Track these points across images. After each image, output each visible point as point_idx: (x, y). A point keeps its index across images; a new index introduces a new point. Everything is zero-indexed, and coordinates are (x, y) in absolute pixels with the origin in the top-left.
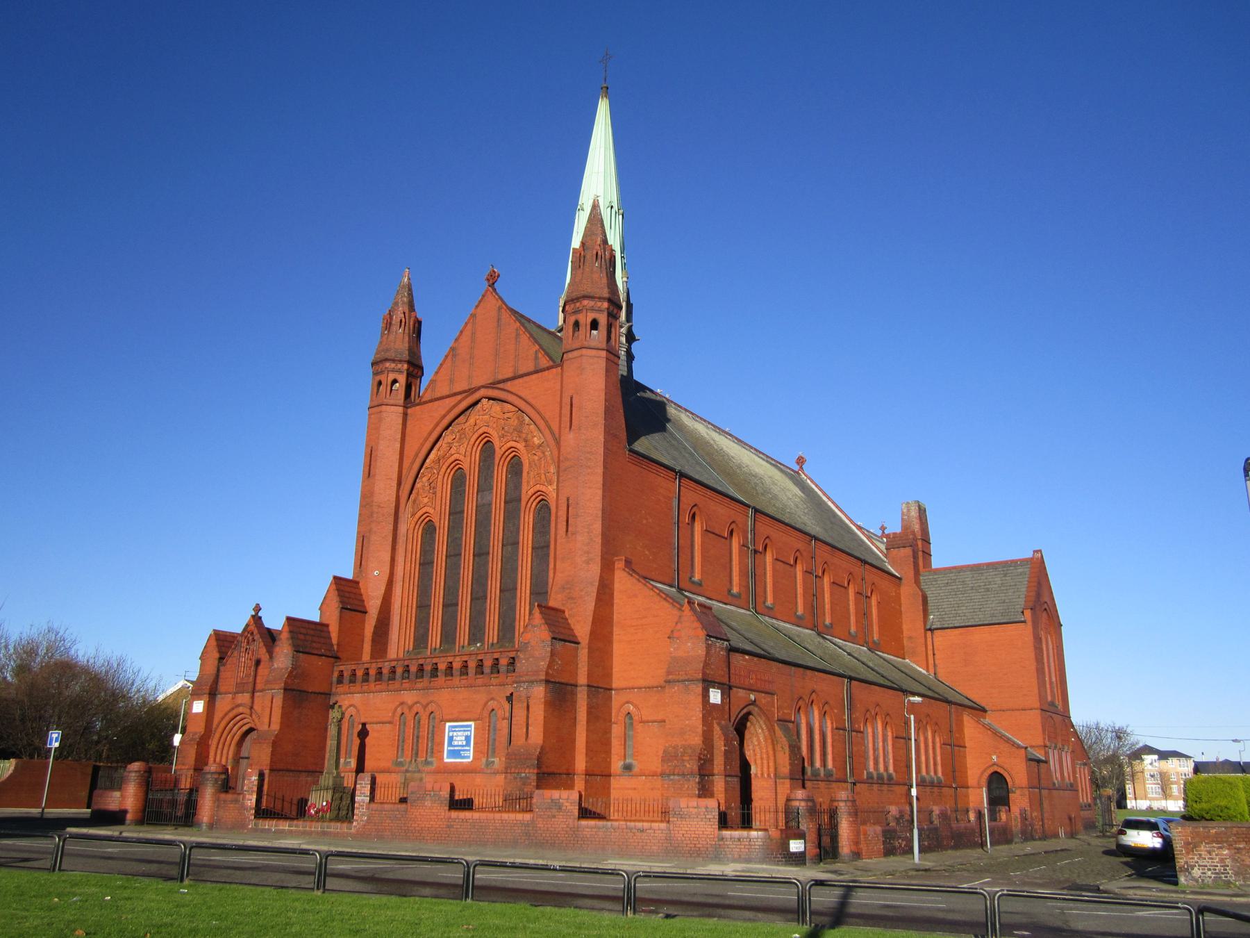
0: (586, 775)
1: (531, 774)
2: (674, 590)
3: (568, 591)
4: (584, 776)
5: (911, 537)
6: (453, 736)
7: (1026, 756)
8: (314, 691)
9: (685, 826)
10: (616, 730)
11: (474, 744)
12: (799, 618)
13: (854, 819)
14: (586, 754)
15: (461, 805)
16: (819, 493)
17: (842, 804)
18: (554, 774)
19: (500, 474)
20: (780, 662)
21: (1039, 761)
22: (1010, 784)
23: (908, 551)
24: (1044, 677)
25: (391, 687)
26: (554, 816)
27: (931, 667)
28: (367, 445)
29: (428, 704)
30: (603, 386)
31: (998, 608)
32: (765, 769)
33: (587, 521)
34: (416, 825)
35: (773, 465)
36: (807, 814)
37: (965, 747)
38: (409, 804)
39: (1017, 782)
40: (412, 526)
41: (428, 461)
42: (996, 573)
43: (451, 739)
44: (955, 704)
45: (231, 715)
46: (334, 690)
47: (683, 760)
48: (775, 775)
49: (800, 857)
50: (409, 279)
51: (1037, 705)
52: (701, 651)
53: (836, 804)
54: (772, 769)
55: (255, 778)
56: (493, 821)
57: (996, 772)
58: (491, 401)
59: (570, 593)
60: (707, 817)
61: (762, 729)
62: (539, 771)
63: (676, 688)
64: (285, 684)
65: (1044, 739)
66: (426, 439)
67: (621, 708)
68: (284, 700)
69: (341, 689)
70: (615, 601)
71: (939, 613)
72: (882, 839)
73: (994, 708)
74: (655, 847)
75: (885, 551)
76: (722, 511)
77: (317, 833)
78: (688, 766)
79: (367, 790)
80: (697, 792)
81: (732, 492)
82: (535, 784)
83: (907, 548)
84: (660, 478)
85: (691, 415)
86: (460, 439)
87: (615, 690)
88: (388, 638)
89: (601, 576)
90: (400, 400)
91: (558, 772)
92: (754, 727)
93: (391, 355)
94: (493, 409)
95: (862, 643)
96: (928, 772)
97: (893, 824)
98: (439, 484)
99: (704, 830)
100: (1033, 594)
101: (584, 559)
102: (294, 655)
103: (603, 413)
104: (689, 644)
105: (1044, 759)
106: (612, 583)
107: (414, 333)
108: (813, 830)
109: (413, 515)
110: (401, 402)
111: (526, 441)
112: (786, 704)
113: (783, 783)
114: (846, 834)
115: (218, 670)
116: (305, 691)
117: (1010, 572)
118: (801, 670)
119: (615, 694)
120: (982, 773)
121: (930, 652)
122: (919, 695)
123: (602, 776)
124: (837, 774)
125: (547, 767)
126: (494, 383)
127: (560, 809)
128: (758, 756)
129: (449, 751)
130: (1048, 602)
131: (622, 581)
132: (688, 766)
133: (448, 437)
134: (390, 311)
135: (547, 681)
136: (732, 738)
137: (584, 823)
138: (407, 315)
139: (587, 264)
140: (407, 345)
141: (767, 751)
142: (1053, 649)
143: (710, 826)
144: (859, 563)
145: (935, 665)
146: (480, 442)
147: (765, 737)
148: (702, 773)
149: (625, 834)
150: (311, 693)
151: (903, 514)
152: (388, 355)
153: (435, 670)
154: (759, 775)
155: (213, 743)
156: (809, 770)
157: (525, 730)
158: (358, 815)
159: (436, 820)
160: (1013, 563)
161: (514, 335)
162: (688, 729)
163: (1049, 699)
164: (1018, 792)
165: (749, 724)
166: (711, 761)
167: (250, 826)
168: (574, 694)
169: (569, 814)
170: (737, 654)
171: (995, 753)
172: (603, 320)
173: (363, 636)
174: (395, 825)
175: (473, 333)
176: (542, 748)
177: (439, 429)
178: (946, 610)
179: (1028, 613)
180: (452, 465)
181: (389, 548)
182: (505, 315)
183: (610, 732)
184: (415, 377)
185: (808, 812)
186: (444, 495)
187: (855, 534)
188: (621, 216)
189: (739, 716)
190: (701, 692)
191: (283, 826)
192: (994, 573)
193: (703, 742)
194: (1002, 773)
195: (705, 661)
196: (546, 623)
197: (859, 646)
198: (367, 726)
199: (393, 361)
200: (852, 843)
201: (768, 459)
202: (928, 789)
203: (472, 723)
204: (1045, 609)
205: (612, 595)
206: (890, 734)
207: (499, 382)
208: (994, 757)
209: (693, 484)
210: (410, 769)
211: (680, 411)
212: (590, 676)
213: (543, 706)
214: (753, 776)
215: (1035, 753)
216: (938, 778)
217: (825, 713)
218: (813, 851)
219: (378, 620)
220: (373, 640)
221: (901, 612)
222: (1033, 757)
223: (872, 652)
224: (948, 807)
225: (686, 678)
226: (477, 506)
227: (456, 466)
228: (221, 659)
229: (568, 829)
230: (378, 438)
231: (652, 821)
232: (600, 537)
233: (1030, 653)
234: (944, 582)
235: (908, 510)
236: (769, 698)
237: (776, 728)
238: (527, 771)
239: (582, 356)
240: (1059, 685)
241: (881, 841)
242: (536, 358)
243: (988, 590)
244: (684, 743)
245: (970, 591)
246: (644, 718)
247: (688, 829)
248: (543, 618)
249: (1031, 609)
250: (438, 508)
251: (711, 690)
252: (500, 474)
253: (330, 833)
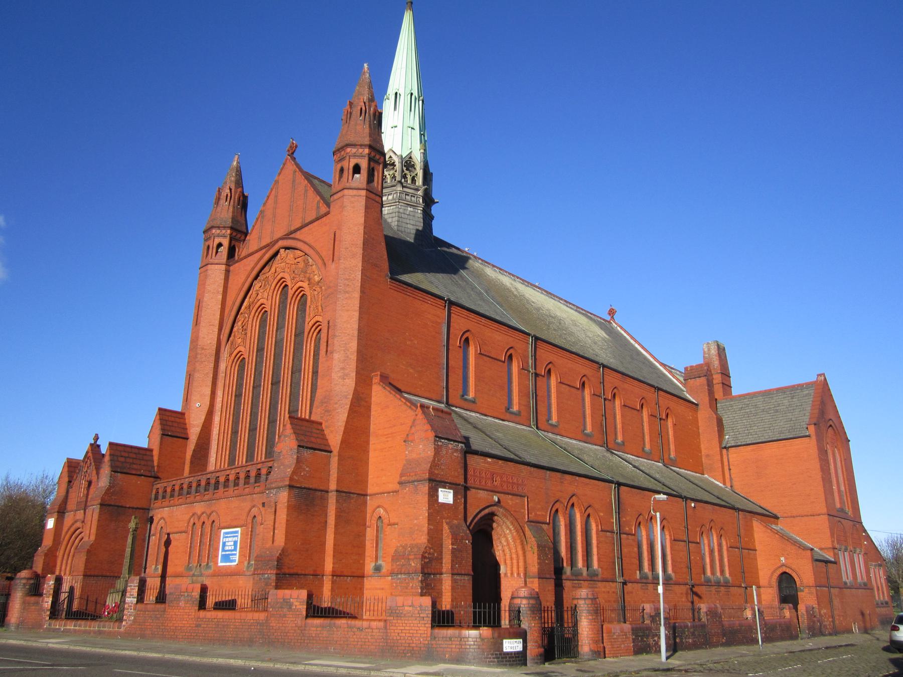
0: (333, 576)
1: (271, 575)
2: (443, 405)
3: (325, 405)
4: (331, 577)
5: (705, 368)
6: (225, 542)
7: (812, 558)
8: (131, 506)
9: (401, 625)
10: (370, 533)
11: (240, 548)
12: (587, 435)
13: (594, 617)
14: (334, 556)
15: (223, 606)
16: (628, 337)
17: (581, 602)
18: (298, 575)
19: (292, 310)
20: (531, 466)
21: (827, 562)
22: (798, 583)
23: (703, 380)
24: (831, 486)
25: (188, 500)
26: (285, 616)
27: (728, 480)
28: (197, 299)
29: (210, 514)
30: (362, 220)
31: (786, 426)
32: (515, 569)
33: (343, 341)
34: (171, 625)
35: (583, 314)
36: (529, 612)
37: (756, 550)
38: (167, 605)
39: (805, 581)
40: (230, 364)
41: (243, 307)
42: (785, 396)
43: (224, 544)
44: (743, 510)
45: (72, 530)
46: (152, 506)
47: (409, 559)
48: (525, 574)
49: (516, 657)
50: (238, 163)
51: (825, 510)
52: (430, 453)
53: (575, 602)
54: (522, 569)
55: (52, 582)
56: (233, 621)
57: (785, 573)
58: (287, 251)
59: (326, 406)
60: (421, 615)
61: (510, 530)
62: (278, 572)
63: (407, 489)
64: (101, 500)
65: (833, 542)
66: (241, 290)
67: (374, 512)
68: (100, 514)
69: (158, 504)
70: (372, 414)
71: (733, 434)
72: (631, 637)
73: (785, 515)
74: (372, 647)
75: (683, 381)
76: (500, 339)
77: (95, 632)
78: (413, 564)
79: (135, 592)
80: (420, 591)
81: (514, 323)
82: (274, 584)
83: (702, 378)
84: (427, 305)
85: (498, 270)
86: (265, 286)
87: (370, 495)
88: (207, 460)
89: (356, 391)
90: (224, 259)
91: (303, 572)
92: (502, 527)
93: (218, 223)
94: (288, 257)
95: (656, 459)
96: (713, 573)
97: (647, 622)
98: (250, 326)
99: (418, 629)
100: (816, 411)
101: (340, 374)
102: (111, 474)
103: (362, 244)
104: (421, 446)
105: (833, 560)
106: (370, 396)
107: (239, 205)
108: (535, 628)
109: (231, 355)
110: (224, 261)
111: (309, 280)
112: (539, 506)
113: (533, 582)
114: (586, 633)
115: (67, 492)
116: (122, 507)
117: (797, 394)
118: (559, 474)
119: (370, 499)
120: (772, 574)
121: (726, 468)
122: (664, 493)
123: (353, 577)
124: (603, 574)
125: (289, 568)
126: (288, 235)
127: (290, 608)
128: (508, 557)
129: (222, 555)
130: (833, 419)
131: (379, 394)
132: (413, 564)
133: (257, 285)
134: (219, 188)
135: (291, 487)
136: (462, 536)
137: (311, 621)
138: (233, 191)
139: (352, 119)
140: (230, 214)
141: (517, 551)
142: (841, 461)
143: (423, 625)
144: (653, 389)
145: (731, 479)
146: (280, 287)
147: (513, 537)
148: (426, 571)
149: (346, 633)
150: (129, 508)
151: (704, 353)
152: (214, 224)
153: (217, 482)
154: (509, 575)
155: (60, 554)
156: (567, 569)
157: (272, 533)
158: (126, 615)
159: (188, 619)
160: (800, 387)
161: (303, 191)
162: (416, 528)
163: (838, 505)
164: (806, 590)
165: (495, 525)
166: (439, 559)
167: (45, 626)
168: (324, 500)
169: (298, 613)
170: (476, 457)
171: (783, 555)
172: (364, 164)
173: (184, 458)
174: (156, 624)
175: (276, 196)
176: (283, 550)
177: (250, 280)
178: (740, 430)
179: (812, 428)
180: (259, 309)
181: (210, 384)
182: (298, 174)
183: (364, 535)
184: (239, 240)
185: (530, 610)
186: (253, 335)
187: (658, 369)
188: (421, 102)
189: (479, 516)
190: (427, 492)
191: (70, 626)
192: (783, 396)
193: (428, 540)
194: (790, 573)
195: (434, 461)
196: (295, 433)
197: (653, 462)
198: (171, 536)
199: (219, 227)
200: (591, 642)
201: (578, 309)
202: (713, 589)
203: (239, 529)
204: (831, 426)
205: (368, 408)
206: (668, 537)
207: (292, 233)
208: (782, 559)
209: (465, 312)
210: (196, 573)
211: (485, 266)
212: (339, 480)
213: (286, 510)
214: (502, 575)
215: (824, 555)
216: (725, 578)
217: (721, 536)
218: (534, 650)
219: (197, 445)
220: (192, 462)
221: (699, 433)
222: (821, 558)
223: (667, 467)
224: (718, 605)
225: (416, 479)
226: (276, 342)
227: (262, 309)
228: (70, 482)
229: (297, 628)
230: (204, 292)
231: (372, 620)
232: (356, 354)
233: (815, 465)
234: (739, 407)
235: (709, 350)
236: (517, 500)
237: (527, 529)
238: (269, 572)
239: (344, 196)
240: (848, 494)
241: (631, 639)
242: (318, 207)
243: (777, 411)
244: (412, 542)
245: (762, 413)
246: (392, 521)
247: (403, 628)
248: (293, 428)
249: (815, 424)
250: (248, 347)
251: (440, 490)
252: (292, 310)
253: (105, 631)
